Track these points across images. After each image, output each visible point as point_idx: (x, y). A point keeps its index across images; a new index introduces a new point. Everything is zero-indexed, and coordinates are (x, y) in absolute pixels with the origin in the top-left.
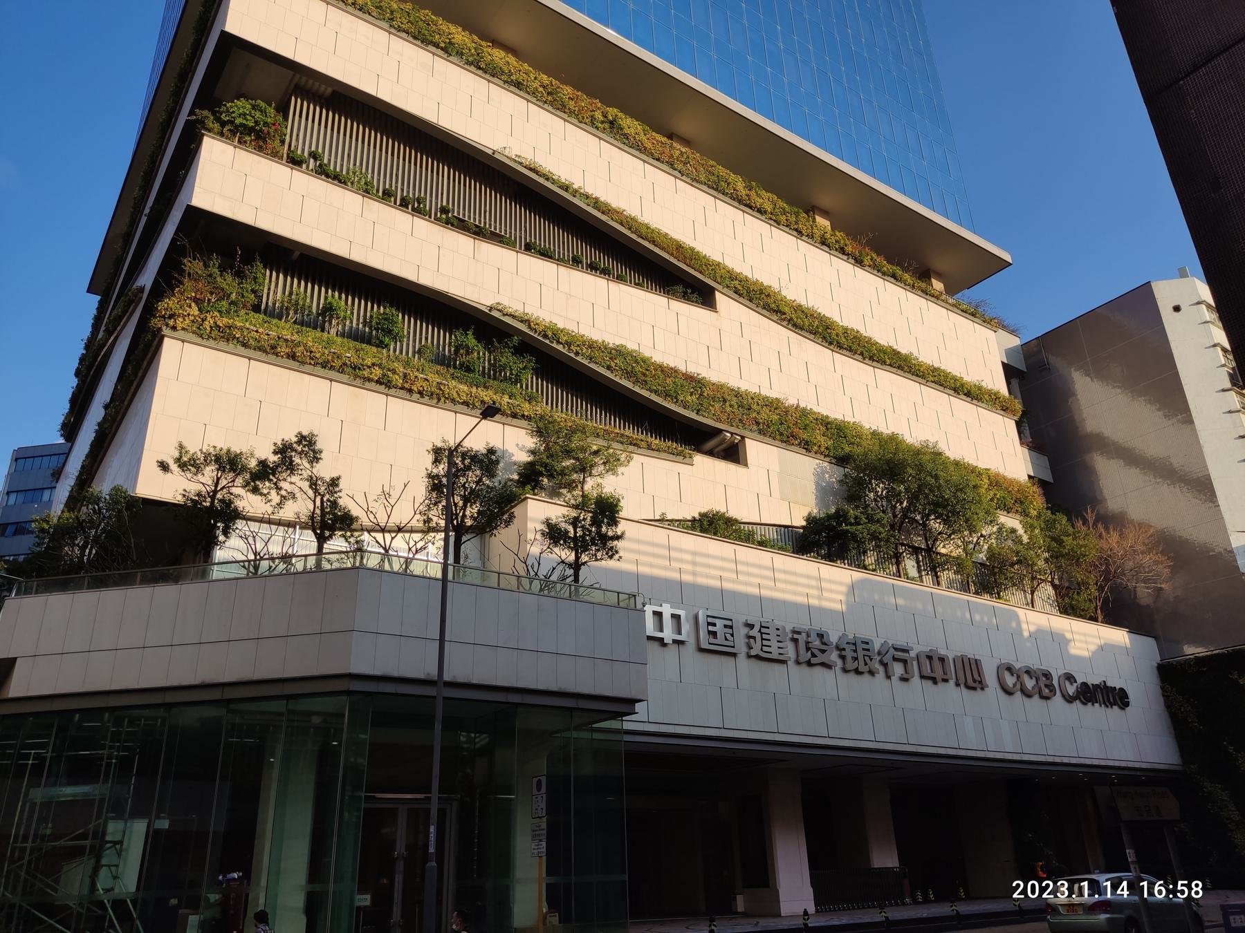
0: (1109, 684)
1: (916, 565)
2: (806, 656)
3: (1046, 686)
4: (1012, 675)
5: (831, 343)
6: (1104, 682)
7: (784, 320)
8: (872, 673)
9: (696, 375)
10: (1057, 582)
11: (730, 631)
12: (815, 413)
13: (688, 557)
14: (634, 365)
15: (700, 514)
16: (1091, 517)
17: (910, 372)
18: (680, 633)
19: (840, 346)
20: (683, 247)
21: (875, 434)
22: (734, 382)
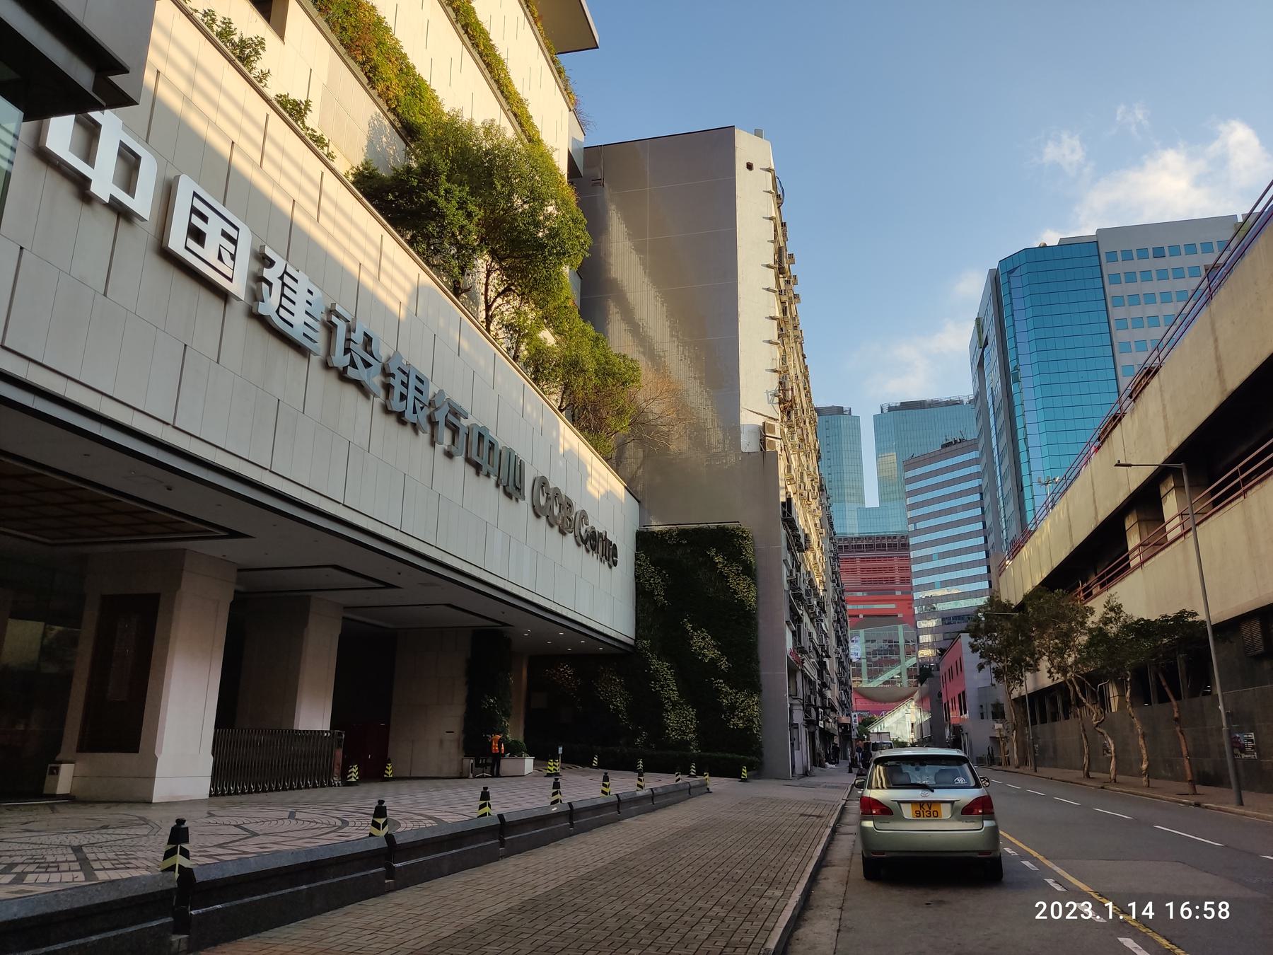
2: (340, 360)
8: (415, 427)
11: (231, 247)
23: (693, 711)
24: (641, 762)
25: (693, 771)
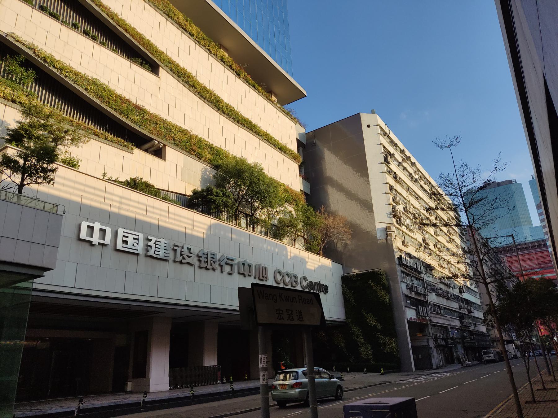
0: (321, 283)
1: (246, 222)
2: (179, 258)
3: (295, 281)
4: (281, 275)
5: (219, 110)
6: (319, 281)
7: (196, 91)
8: (214, 269)
9: (141, 107)
10: (306, 237)
11: (137, 241)
12: (206, 141)
13: (118, 199)
14: (103, 91)
15: (131, 179)
16: (323, 210)
17: (256, 132)
18: (104, 239)
19: (223, 112)
20: (143, 38)
21: (234, 157)
22: (163, 115)
23: (370, 346)
24: (225, 378)
25: (365, 371)
